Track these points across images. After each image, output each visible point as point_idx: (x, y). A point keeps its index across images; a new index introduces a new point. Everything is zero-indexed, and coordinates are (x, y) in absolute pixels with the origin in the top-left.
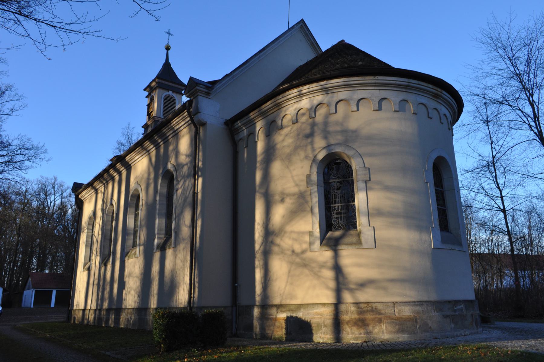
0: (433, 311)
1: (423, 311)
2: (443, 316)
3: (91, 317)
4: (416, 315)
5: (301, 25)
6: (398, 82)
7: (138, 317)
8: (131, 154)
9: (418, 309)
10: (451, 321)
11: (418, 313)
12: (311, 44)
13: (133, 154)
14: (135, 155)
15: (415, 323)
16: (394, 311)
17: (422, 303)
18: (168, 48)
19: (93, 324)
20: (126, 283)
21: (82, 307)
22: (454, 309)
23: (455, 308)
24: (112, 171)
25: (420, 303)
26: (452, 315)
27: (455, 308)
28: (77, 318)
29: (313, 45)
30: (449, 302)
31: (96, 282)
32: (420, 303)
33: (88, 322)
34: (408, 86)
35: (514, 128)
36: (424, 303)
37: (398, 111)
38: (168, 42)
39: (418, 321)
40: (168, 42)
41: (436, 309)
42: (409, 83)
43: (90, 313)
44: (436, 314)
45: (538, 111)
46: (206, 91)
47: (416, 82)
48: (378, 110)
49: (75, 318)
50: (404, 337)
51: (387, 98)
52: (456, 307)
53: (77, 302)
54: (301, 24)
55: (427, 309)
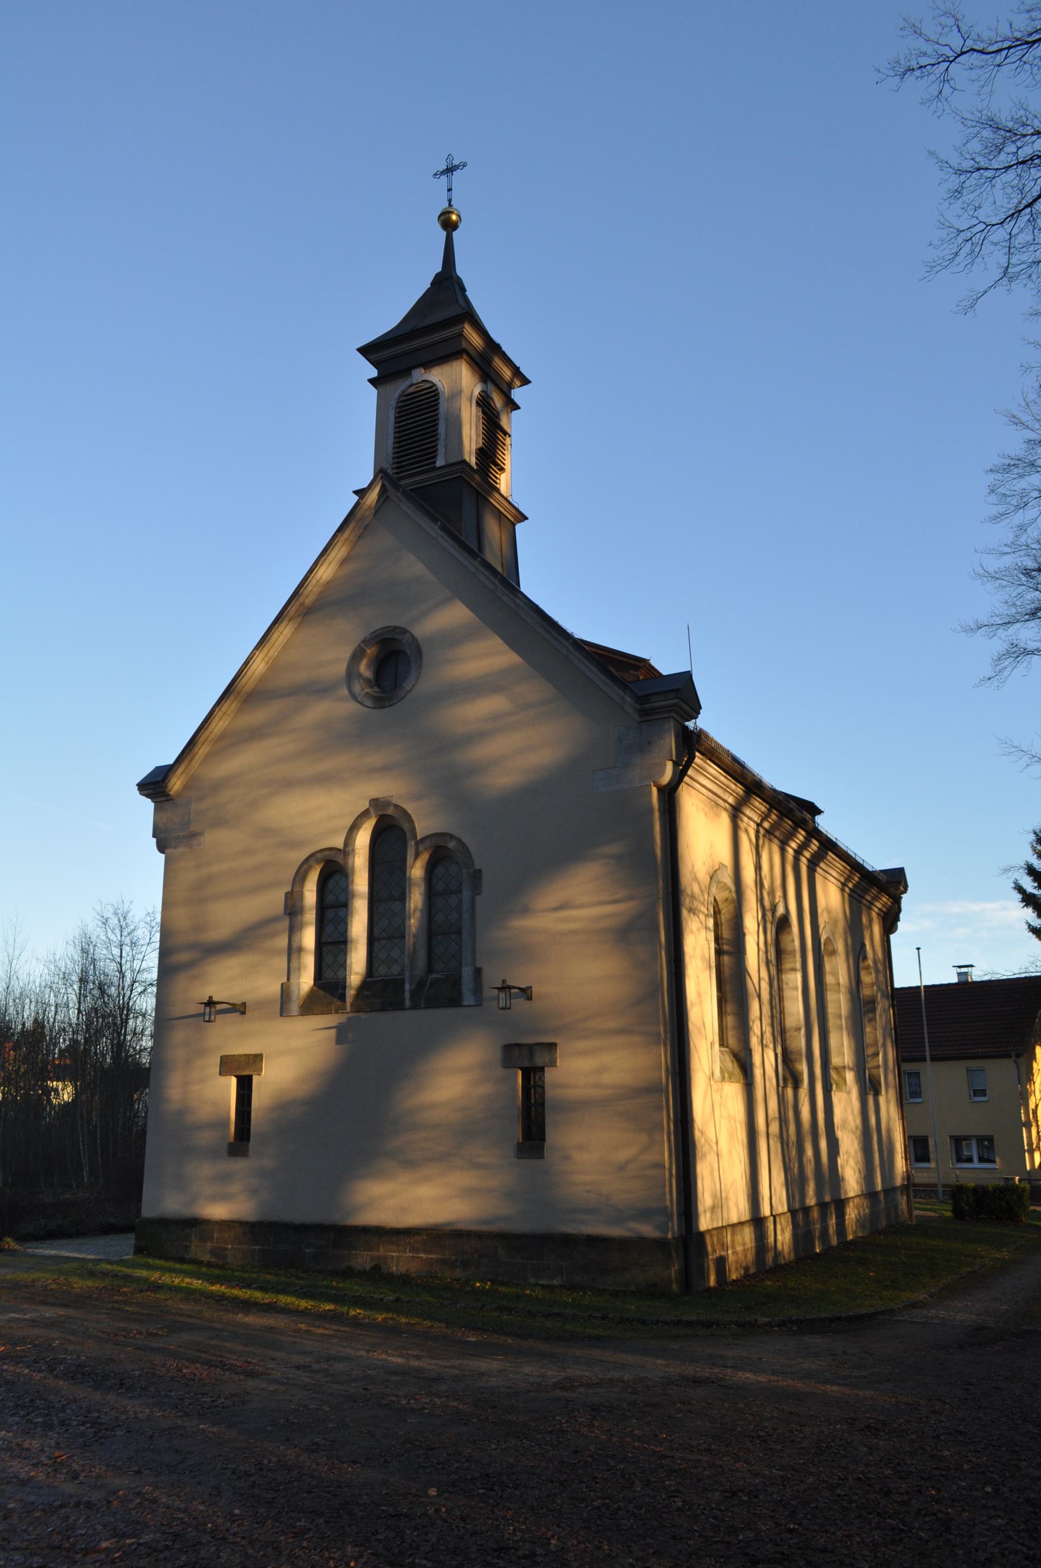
3: (782, 1236)
7: (812, 1227)
8: (837, 859)
13: (839, 864)
14: (841, 870)
18: (448, 225)
20: (840, 1142)
21: (738, 1209)
24: (815, 845)
28: (731, 1258)
31: (775, 1128)
33: (777, 1254)
35: (119, 959)
38: (450, 201)
40: (450, 201)
43: (779, 1227)
45: (894, 1069)
49: (721, 1261)
53: (714, 1196)
54: (380, 476)
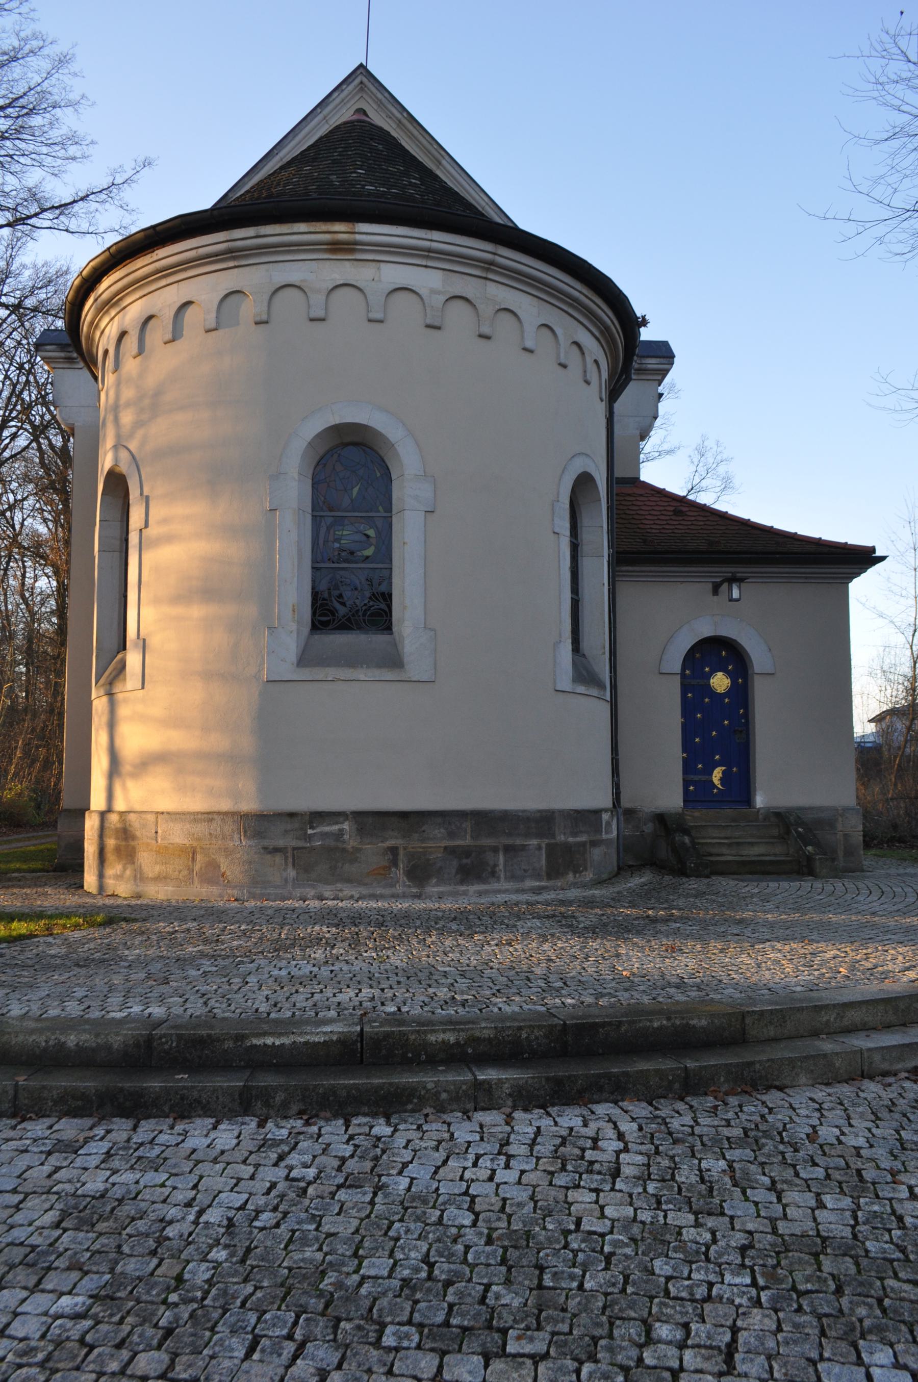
0: (236, 836)
1: (210, 834)
2: (265, 848)
4: (195, 844)
5: (361, 83)
6: (202, 251)
9: (200, 829)
10: (290, 860)
11: (199, 839)
12: (398, 126)
15: (190, 863)
16: (156, 832)
17: (210, 816)
19: (609, 813)
22: (306, 833)
23: (310, 832)
25: (209, 816)
26: (294, 849)
27: (310, 832)
29: (404, 125)
30: (292, 815)
32: (206, 816)
34: (232, 252)
36: (215, 816)
37: (216, 329)
39: (199, 857)
41: (245, 832)
42: (229, 243)
44: (244, 843)
46: (62, 354)
47: (250, 231)
48: (173, 340)
50: (167, 891)
51: (192, 300)
52: (312, 828)
55: (222, 830)
